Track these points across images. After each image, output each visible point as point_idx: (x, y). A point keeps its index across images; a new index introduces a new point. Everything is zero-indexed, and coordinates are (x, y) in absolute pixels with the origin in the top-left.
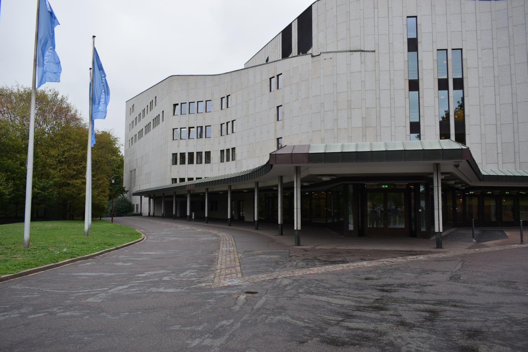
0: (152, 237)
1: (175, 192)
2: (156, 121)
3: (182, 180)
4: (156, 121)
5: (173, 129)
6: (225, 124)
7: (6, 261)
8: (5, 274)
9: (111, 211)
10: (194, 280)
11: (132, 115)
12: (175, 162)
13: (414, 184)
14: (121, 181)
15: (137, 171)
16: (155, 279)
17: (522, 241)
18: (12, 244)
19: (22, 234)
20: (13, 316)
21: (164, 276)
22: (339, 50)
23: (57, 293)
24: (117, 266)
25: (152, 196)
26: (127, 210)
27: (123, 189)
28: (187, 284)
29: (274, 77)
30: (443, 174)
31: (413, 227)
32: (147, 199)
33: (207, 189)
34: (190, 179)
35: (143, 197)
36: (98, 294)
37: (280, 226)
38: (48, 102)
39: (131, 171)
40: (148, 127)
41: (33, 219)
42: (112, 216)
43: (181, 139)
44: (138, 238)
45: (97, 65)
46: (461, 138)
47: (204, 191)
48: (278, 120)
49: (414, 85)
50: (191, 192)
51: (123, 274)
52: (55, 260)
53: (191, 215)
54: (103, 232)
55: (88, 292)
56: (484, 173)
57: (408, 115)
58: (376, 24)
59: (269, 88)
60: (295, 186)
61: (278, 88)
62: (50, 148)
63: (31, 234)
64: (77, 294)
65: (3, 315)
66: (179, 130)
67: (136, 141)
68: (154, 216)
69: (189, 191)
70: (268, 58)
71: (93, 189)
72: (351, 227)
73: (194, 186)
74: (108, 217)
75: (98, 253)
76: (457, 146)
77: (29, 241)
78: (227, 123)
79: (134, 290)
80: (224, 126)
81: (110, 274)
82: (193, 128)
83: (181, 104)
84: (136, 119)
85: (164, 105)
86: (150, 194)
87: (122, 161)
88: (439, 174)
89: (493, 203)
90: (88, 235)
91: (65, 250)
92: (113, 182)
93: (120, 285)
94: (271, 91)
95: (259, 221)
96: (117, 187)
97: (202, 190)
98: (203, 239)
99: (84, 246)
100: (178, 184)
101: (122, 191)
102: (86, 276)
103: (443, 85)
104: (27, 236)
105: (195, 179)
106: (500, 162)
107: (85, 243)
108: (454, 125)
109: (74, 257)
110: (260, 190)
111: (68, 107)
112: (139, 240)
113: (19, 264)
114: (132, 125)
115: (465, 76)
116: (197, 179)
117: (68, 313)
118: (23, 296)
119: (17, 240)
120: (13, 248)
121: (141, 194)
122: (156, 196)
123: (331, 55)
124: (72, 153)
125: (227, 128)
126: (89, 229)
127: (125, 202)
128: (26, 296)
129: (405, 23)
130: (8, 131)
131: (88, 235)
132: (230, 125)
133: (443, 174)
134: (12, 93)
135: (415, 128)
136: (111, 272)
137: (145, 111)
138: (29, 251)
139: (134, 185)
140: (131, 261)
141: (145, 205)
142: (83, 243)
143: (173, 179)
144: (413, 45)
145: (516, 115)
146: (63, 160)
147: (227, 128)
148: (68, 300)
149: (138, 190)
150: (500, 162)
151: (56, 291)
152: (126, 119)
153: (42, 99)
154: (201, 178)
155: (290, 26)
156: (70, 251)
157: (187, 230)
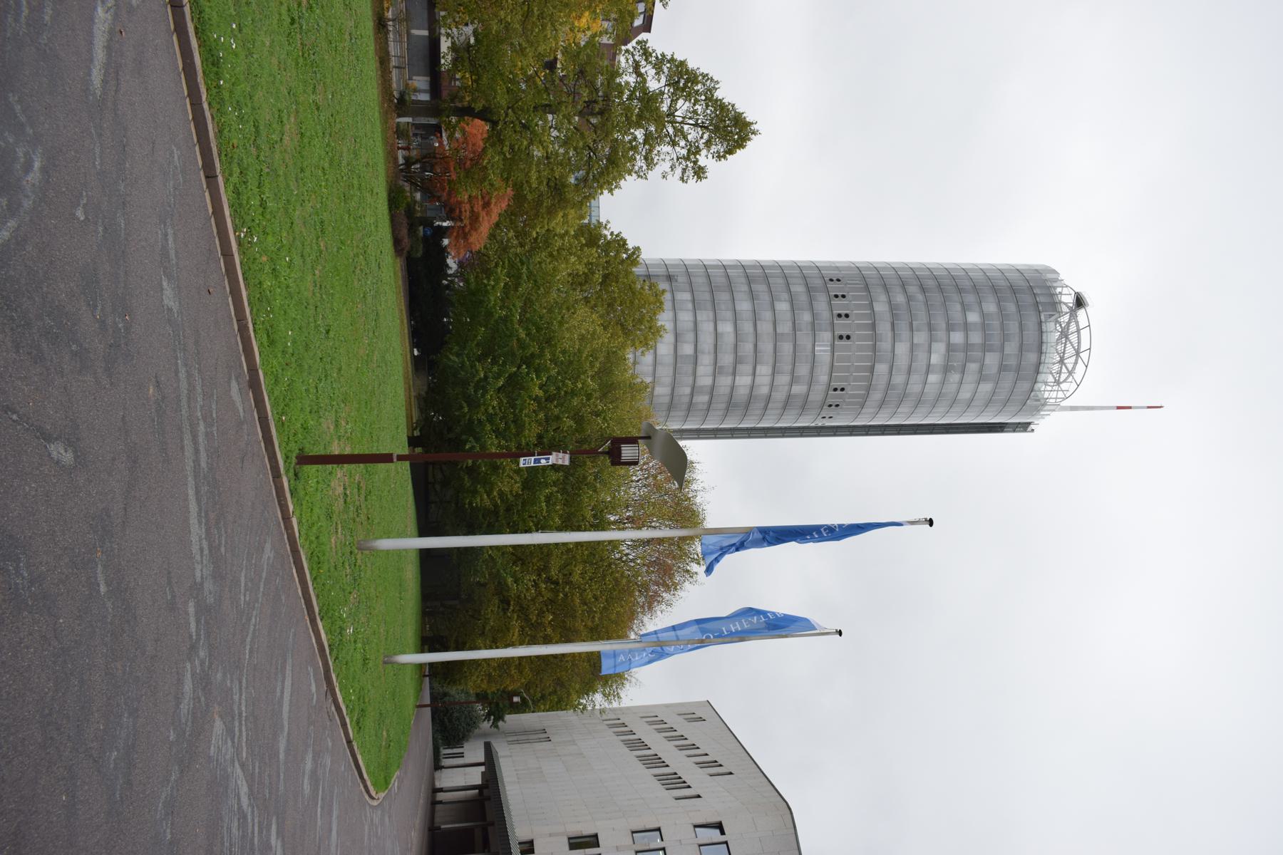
0: (376, 820)
1: (492, 824)
2: (674, 782)
4: (674, 782)
5: (659, 829)
7: (329, 516)
11: (681, 719)
14: (522, 708)
15: (545, 745)
19: (388, 535)
20: (198, 567)
25: (486, 792)
26: (449, 729)
32: (478, 781)
35: (482, 769)
40: (655, 761)
41: (425, 554)
45: (780, 625)
63: (388, 552)
64: (236, 689)
65: (202, 550)
66: (659, 843)
67: (618, 734)
68: (434, 803)
75: (340, 700)
79: (234, 831)
83: (726, 843)
84: (672, 730)
85: (716, 799)
90: (385, 663)
92: (516, 699)
96: (499, 706)
101: (496, 715)
102: (282, 693)
104: (386, 544)
109: (331, 650)
112: (371, 788)
113: (320, 544)
114: (655, 719)
117: (188, 686)
122: (487, 803)
128: (243, 579)
136: (287, 751)
137: (694, 750)
139: (511, 743)
140: (315, 790)
141: (461, 777)
142: (365, 659)
148: (224, 674)
151: (249, 639)
152: (667, 706)
153: (678, 549)
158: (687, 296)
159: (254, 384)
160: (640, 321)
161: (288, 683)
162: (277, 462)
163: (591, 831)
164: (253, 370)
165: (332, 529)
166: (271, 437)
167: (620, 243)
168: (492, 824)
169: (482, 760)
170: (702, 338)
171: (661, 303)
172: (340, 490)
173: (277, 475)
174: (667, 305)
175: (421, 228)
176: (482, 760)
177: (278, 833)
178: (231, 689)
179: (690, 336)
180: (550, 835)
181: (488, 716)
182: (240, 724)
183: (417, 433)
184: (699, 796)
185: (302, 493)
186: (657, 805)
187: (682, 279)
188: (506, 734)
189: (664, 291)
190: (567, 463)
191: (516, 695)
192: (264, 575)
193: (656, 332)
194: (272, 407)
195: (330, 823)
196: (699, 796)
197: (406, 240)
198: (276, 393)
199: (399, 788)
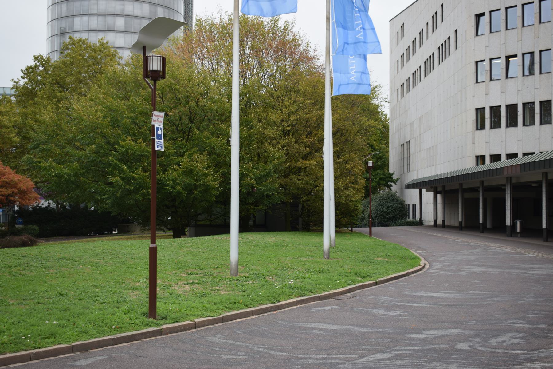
0: (439, 266)
1: (461, 185)
2: (444, 49)
3: (496, 158)
4: (444, 49)
5: (477, 63)
7: (204, 295)
8: (201, 316)
9: (370, 216)
10: (518, 354)
11: (401, 42)
12: (480, 125)
14: (386, 165)
16: (443, 346)
18: (214, 268)
21: (460, 342)
23: (273, 356)
24: (375, 315)
25: (440, 189)
26: (396, 214)
27: (390, 176)
28: (503, 361)
32: (431, 194)
33: (546, 174)
34: (511, 156)
35: (424, 191)
36: (339, 364)
38: (264, 35)
39: (402, 145)
40: (429, 63)
41: (244, 228)
42: (372, 224)
43: (491, 80)
44: (413, 266)
47: (539, 177)
50: (514, 181)
51: (385, 330)
52: (274, 298)
53: (514, 225)
54: (354, 252)
55: (324, 359)
62: (270, 109)
64: (304, 362)
66: (486, 63)
68: (444, 226)
69: (509, 179)
71: (336, 178)
73: (518, 169)
74: (365, 226)
75: (343, 289)
77: (238, 263)
79: (403, 363)
81: (362, 330)
82: (516, 56)
83: (491, 12)
86: (436, 185)
87: (386, 127)
90: (328, 258)
91: (291, 281)
92: (370, 164)
93: (378, 352)
96: (378, 174)
97: (535, 176)
98: (537, 272)
99: (322, 276)
100: (488, 165)
101: (388, 179)
102: (321, 329)
104: (234, 256)
105: (520, 155)
107: (323, 272)
109: (304, 295)
111: (294, 40)
113: (221, 302)
116: (524, 154)
118: (223, 357)
119: (223, 262)
120: (215, 275)
121: (420, 185)
122: (447, 189)
124: (302, 115)
126: (331, 246)
127: (393, 200)
130: (208, 88)
131: (328, 258)
134: (213, 25)
136: (364, 326)
138: (237, 280)
139: (408, 171)
140: (399, 307)
141: (428, 206)
142: (320, 271)
143: (477, 157)
146: (289, 128)
149: (415, 178)
151: (273, 353)
154: (534, 153)
156: (299, 284)
157: (508, 253)
158: (77, 20)
159: (84, 348)
160: (94, 58)
161: (316, 325)
162: (149, 332)
163: (473, 113)
164: (72, 349)
165: (216, 293)
166: (129, 336)
167: (30, 72)
168: (461, 185)
169: (417, 191)
170: (111, 10)
171: (80, 40)
172: (187, 288)
173: (160, 332)
174: (84, 36)
175: (17, 226)
176: (417, 191)
177: (418, 333)
178: (302, 365)
179: (110, 19)
180: (473, 143)
181: (389, 186)
182: (331, 359)
183: (171, 233)
184: (456, 31)
185: (178, 314)
186: (459, 62)
187: (63, 24)
188: (402, 174)
189: (71, 38)
190: (163, 114)
191: (367, 163)
192: (230, 342)
193: (104, 47)
194: (105, 335)
195: (427, 297)
196: (456, 31)
197: (23, 238)
198: (94, 332)
199: (424, 250)
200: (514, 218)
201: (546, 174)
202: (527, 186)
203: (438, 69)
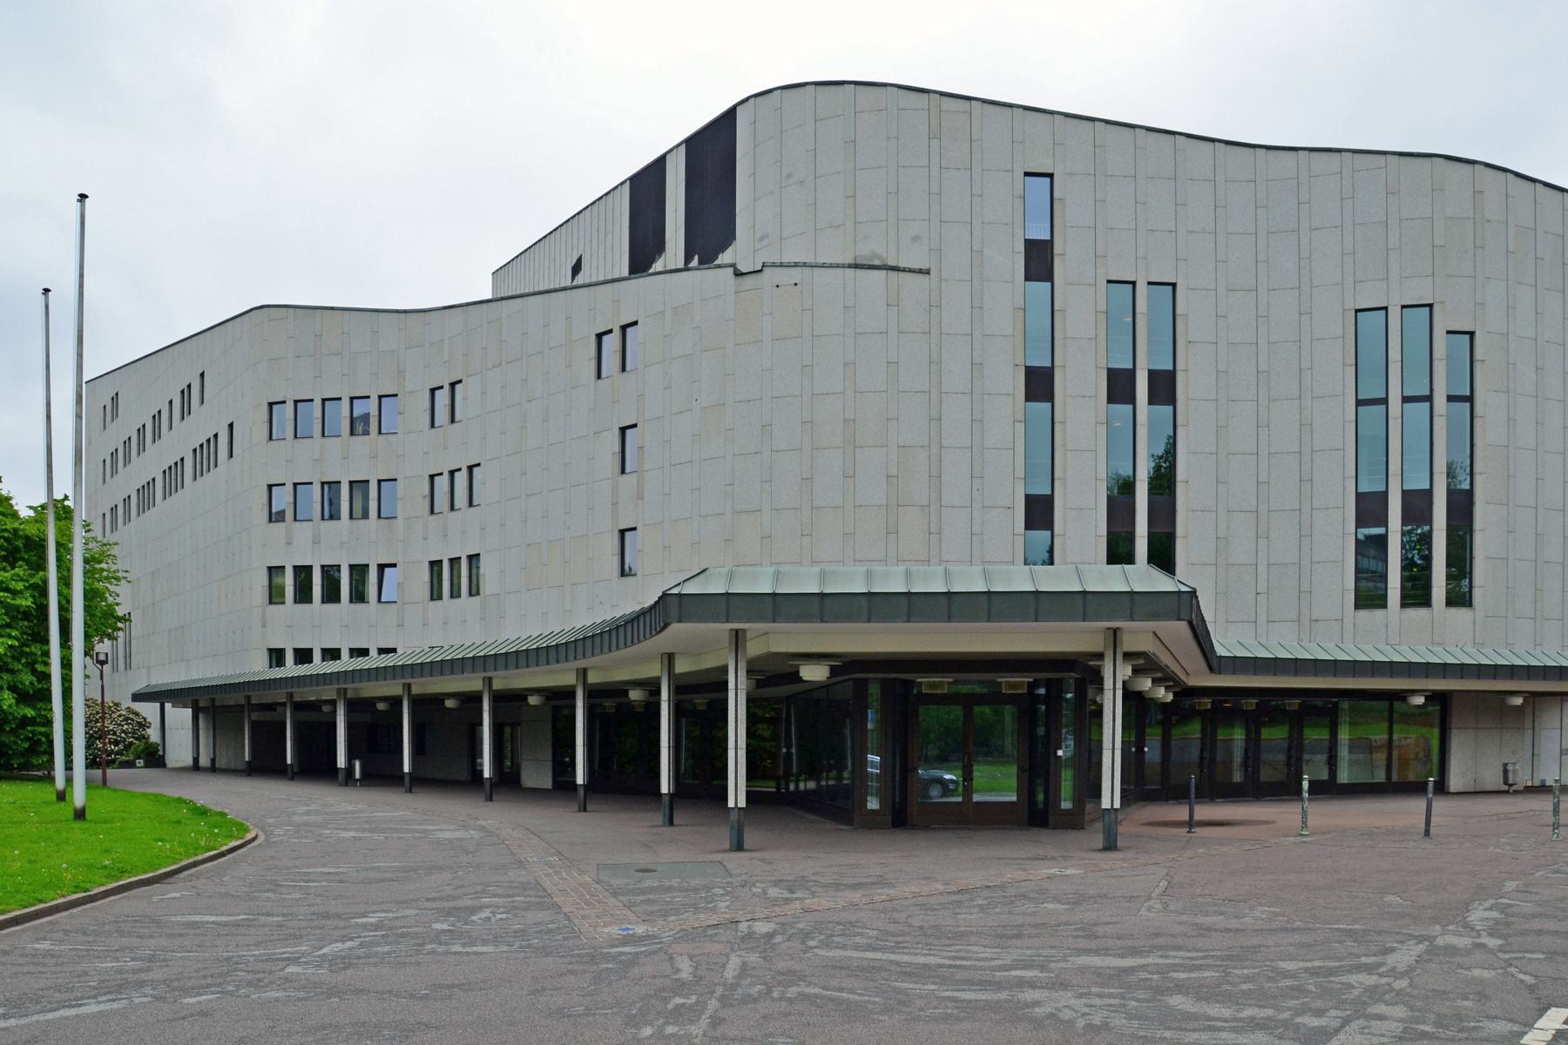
2: (206, 454)
3: (303, 656)
4: (206, 454)
6: (446, 478)
11: (111, 427)
13: (1049, 684)
17: (1406, 400)
22: (820, 261)
29: (610, 331)
30: (1128, 656)
31: (1041, 797)
37: (666, 800)
40: (173, 474)
46: (1163, 556)
48: (623, 471)
49: (1039, 384)
56: (1221, 651)
57: (1020, 473)
58: (934, 189)
59: (593, 364)
60: (731, 685)
61: (624, 369)
68: (213, 769)
70: (579, 261)
72: (873, 804)
76: (1160, 582)
78: (452, 473)
80: (442, 483)
85: (234, 403)
88: (1119, 657)
89: (1239, 735)
94: (599, 376)
95: (588, 787)
98: (447, 835)
100: (291, 669)
103: (1120, 386)
106: (1262, 619)
108: (1145, 516)
110: (594, 693)
115: (1180, 365)
116: (382, 651)
121: (160, 696)
123: (796, 275)
125: (454, 487)
129: (1019, 191)
132: (462, 478)
133: (1128, 656)
135: (1039, 512)
141: (178, 731)
143: (271, 651)
144: (1039, 260)
145: (1308, 485)
147: (454, 487)
150: (1262, 619)
155: (659, 164)
200: (351, 757)
201: (409, 686)
202: (314, 706)
203: (191, 488)
